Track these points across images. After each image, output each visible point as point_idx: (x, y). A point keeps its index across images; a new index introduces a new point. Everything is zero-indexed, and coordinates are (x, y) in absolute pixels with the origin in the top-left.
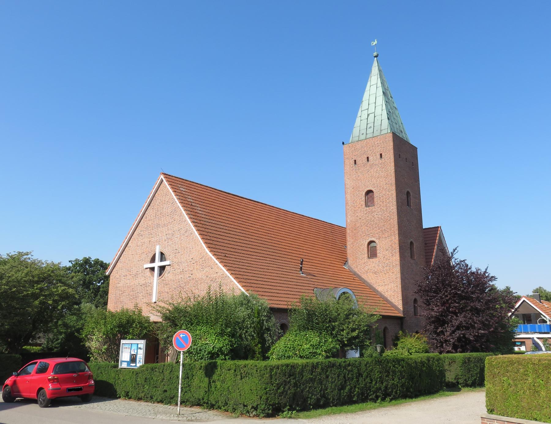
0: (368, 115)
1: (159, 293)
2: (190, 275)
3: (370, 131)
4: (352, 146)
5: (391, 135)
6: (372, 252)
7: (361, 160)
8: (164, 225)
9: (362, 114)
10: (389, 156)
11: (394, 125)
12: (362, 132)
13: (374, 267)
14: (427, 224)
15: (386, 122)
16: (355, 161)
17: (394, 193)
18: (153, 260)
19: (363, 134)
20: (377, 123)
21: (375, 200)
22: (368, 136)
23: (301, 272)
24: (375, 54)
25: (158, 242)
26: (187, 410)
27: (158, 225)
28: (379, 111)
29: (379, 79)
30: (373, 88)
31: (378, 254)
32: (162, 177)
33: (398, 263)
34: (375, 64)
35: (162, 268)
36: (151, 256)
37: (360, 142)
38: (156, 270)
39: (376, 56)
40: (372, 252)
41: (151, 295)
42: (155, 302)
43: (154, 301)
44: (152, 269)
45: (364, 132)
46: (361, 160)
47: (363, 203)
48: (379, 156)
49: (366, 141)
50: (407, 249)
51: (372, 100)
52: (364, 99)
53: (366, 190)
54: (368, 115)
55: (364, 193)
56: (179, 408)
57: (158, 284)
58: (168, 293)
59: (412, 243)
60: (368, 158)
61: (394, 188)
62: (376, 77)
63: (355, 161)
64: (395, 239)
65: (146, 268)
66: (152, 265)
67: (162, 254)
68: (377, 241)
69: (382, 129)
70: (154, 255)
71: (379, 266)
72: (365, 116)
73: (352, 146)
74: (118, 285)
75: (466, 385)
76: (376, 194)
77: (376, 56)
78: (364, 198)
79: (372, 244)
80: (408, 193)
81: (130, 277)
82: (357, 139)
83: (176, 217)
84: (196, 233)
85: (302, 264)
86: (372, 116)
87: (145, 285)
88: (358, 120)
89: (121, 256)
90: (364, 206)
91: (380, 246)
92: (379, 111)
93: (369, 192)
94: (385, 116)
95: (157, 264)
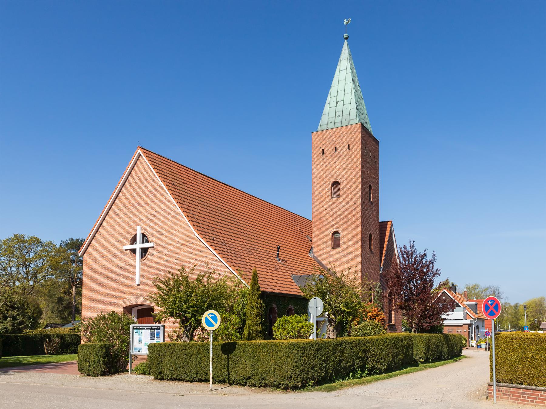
0: (337, 103)
1: (142, 275)
2: (177, 258)
3: (338, 120)
4: (321, 135)
5: (359, 126)
6: (336, 243)
7: (329, 150)
8: (145, 204)
9: (331, 101)
10: (357, 148)
11: (361, 115)
12: (331, 120)
13: (337, 256)
14: (382, 218)
15: (354, 112)
16: (323, 150)
17: (359, 185)
18: (133, 241)
19: (331, 122)
20: (346, 112)
21: (341, 191)
22: (337, 125)
23: (278, 259)
24: (346, 35)
25: (139, 223)
26: (218, 386)
27: (138, 205)
28: (347, 99)
29: (349, 64)
30: (343, 73)
31: (341, 245)
32: (140, 151)
33: (360, 253)
34: (345, 47)
35: (145, 251)
36: (131, 237)
37: (329, 131)
38: (138, 252)
39: (346, 38)
40: (336, 243)
41: (133, 277)
42: (138, 285)
43: (137, 283)
44: (134, 251)
45: (333, 121)
46: (329, 150)
47: (330, 194)
48: (347, 147)
49: (334, 130)
50: (366, 239)
51: (341, 87)
52: (333, 85)
53: (332, 181)
54: (337, 103)
55: (331, 184)
56: (211, 386)
57: (141, 266)
58: (152, 275)
59: (370, 235)
60: (336, 148)
61: (359, 180)
62: (346, 61)
63: (323, 150)
64: (358, 230)
65: (126, 250)
66: (132, 247)
67: (143, 235)
68: (341, 232)
69: (351, 119)
70: (136, 235)
71: (341, 256)
72: (333, 104)
73: (321, 135)
74: (94, 267)
75: (427, 361)
76: (341, 186)
77: (346, 38)
78: (330, 189)
79: (336, 235)
80: (370, 186)
81: (108, 258)
82: (325, 127)
83: (157, 196)
84: (183, 215)
85: (278, 251)
86: (340, 104)
87: (126, 267)
88: (326, 107)
89: (94, 236)
90: (330, 197)
91: (344, 237)
92: (347, 99)
93: (336, 183)
94: (354, 105)
95: (138, 246)
